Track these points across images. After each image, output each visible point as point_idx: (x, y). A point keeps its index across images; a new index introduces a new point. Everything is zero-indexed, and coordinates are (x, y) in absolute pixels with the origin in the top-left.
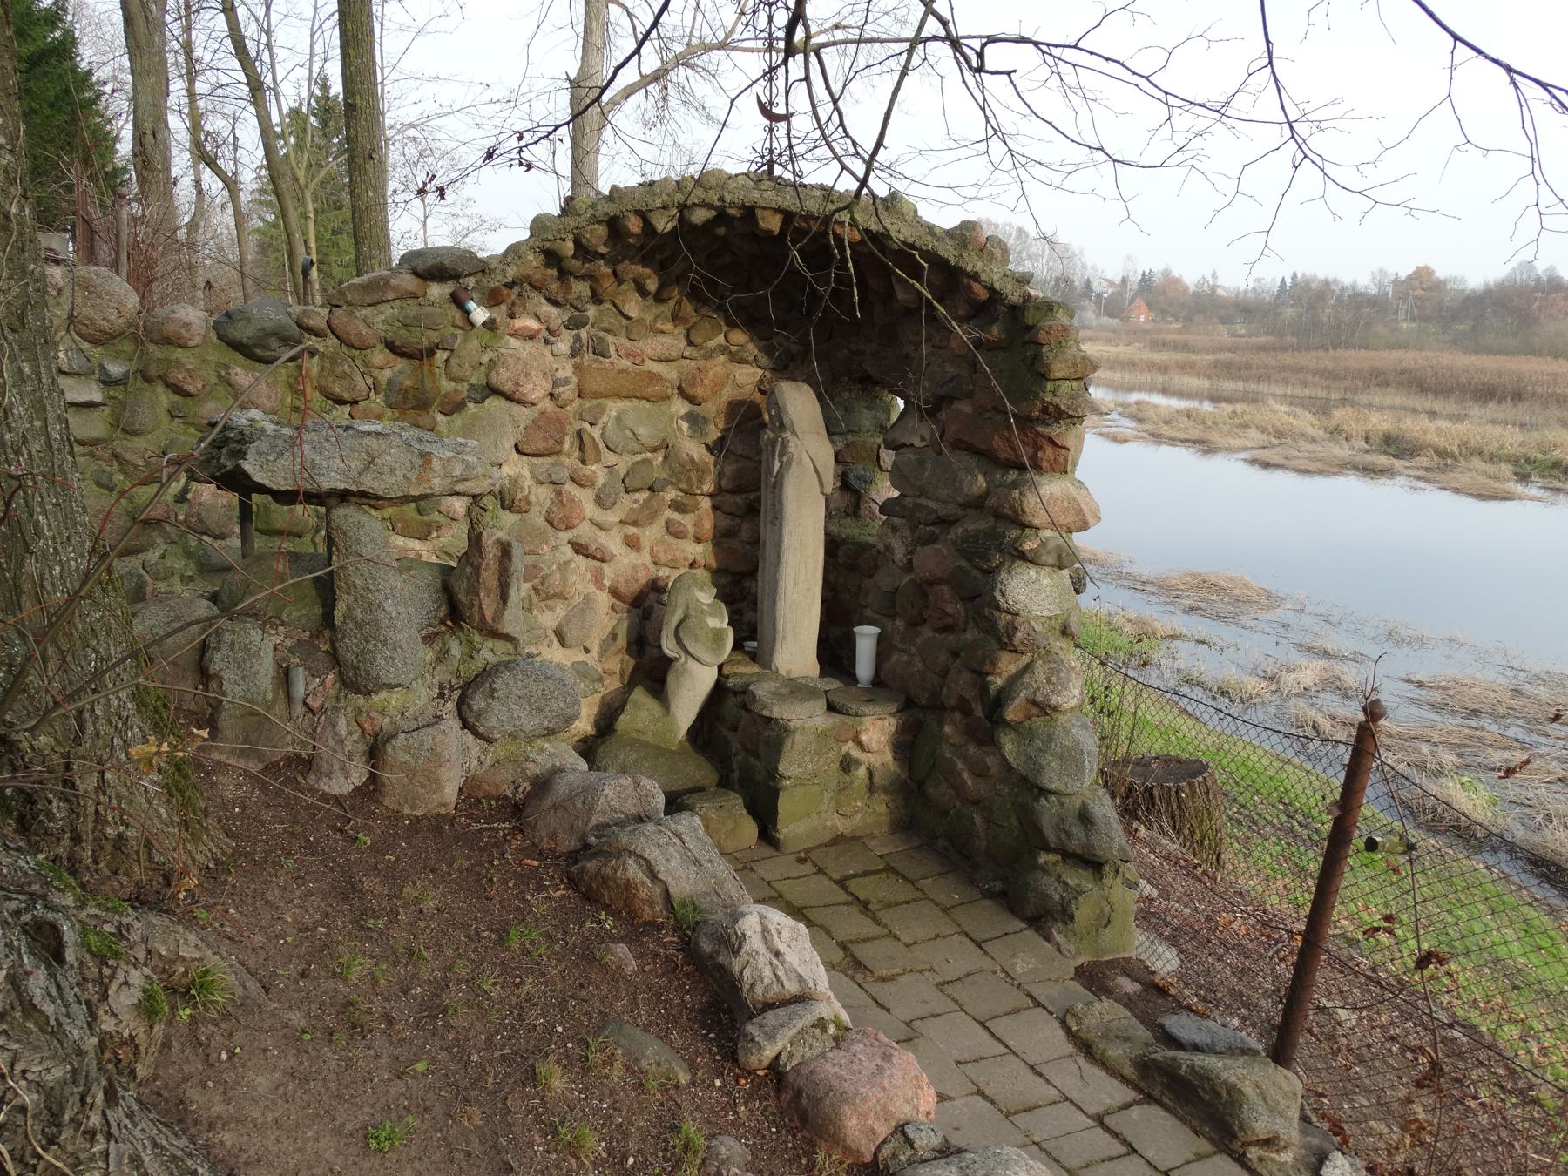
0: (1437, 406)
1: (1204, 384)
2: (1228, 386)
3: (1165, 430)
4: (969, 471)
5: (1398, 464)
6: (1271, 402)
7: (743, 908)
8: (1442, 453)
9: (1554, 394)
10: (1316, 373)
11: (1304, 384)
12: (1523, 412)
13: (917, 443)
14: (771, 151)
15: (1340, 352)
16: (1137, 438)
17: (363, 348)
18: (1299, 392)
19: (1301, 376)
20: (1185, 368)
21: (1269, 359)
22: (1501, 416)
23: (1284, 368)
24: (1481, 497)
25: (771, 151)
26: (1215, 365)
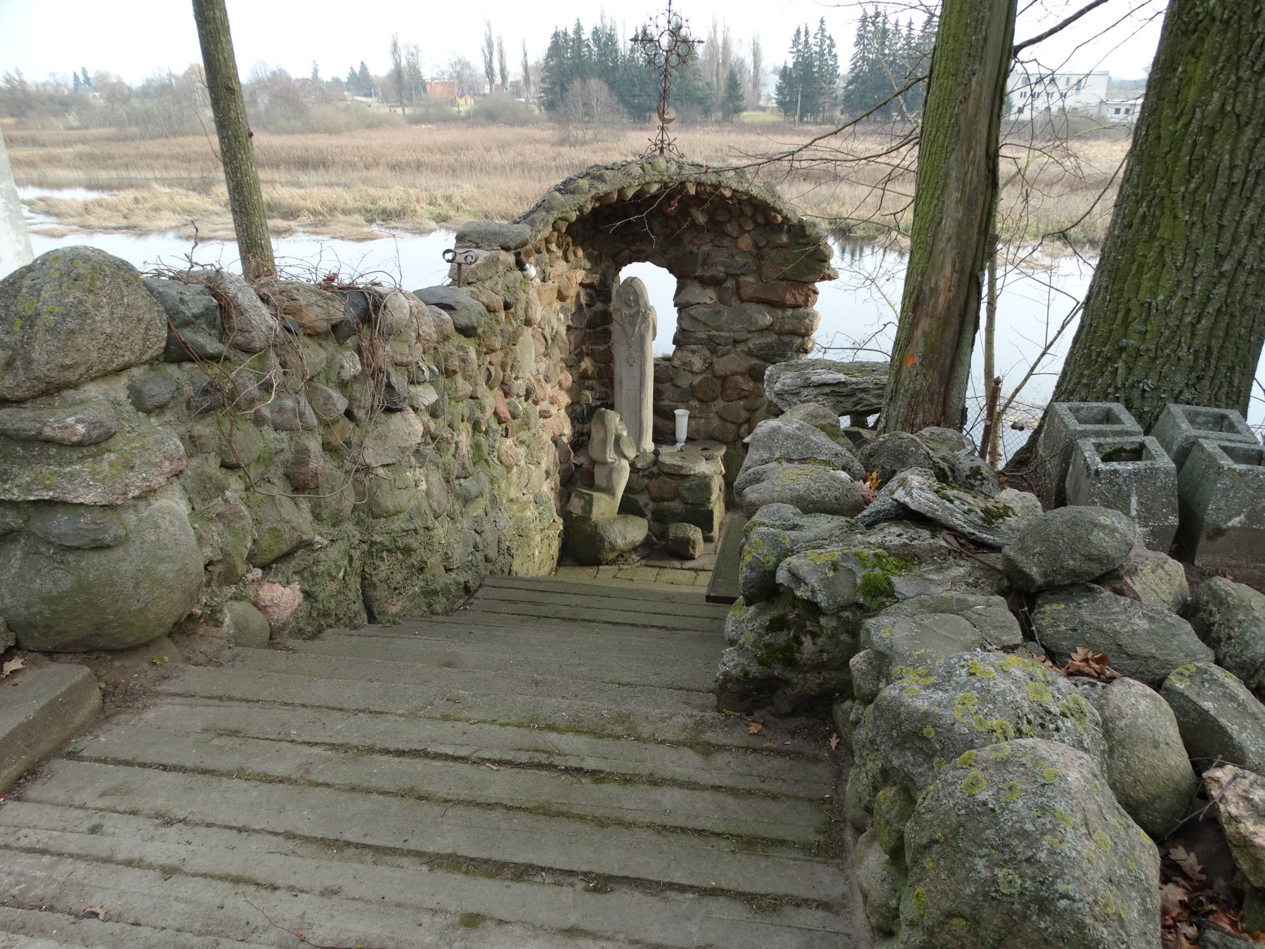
0: (276, 176)
1: (80, 175)
2: (103, 175)
3: (92, 220)
4: (760, 313)
5: (293, 224)
6: (155, 186)
7: (730, 515)
8: (314, 213)
9: (346, 161)
10: (172, 158)
11: (166, 168)
12: (332, 175)
13: (708, 301)
14: (662, 142)
15: (181, 140)
16: (72, 231)
17: (495, 311)
18: (165, 175)
19: (161, 161)
20: (52, 161)
21: (114, 149)
22: (334, 179)
23: (142, 156)
24: (358, 240)
25: (662, 142)
26: (80, 156)
